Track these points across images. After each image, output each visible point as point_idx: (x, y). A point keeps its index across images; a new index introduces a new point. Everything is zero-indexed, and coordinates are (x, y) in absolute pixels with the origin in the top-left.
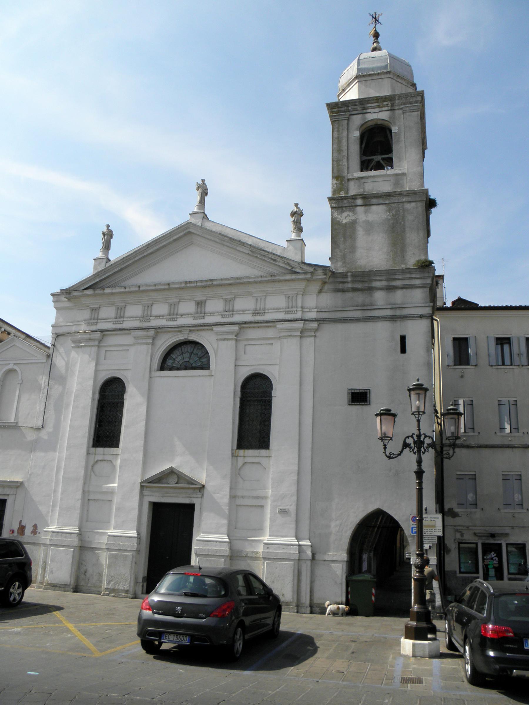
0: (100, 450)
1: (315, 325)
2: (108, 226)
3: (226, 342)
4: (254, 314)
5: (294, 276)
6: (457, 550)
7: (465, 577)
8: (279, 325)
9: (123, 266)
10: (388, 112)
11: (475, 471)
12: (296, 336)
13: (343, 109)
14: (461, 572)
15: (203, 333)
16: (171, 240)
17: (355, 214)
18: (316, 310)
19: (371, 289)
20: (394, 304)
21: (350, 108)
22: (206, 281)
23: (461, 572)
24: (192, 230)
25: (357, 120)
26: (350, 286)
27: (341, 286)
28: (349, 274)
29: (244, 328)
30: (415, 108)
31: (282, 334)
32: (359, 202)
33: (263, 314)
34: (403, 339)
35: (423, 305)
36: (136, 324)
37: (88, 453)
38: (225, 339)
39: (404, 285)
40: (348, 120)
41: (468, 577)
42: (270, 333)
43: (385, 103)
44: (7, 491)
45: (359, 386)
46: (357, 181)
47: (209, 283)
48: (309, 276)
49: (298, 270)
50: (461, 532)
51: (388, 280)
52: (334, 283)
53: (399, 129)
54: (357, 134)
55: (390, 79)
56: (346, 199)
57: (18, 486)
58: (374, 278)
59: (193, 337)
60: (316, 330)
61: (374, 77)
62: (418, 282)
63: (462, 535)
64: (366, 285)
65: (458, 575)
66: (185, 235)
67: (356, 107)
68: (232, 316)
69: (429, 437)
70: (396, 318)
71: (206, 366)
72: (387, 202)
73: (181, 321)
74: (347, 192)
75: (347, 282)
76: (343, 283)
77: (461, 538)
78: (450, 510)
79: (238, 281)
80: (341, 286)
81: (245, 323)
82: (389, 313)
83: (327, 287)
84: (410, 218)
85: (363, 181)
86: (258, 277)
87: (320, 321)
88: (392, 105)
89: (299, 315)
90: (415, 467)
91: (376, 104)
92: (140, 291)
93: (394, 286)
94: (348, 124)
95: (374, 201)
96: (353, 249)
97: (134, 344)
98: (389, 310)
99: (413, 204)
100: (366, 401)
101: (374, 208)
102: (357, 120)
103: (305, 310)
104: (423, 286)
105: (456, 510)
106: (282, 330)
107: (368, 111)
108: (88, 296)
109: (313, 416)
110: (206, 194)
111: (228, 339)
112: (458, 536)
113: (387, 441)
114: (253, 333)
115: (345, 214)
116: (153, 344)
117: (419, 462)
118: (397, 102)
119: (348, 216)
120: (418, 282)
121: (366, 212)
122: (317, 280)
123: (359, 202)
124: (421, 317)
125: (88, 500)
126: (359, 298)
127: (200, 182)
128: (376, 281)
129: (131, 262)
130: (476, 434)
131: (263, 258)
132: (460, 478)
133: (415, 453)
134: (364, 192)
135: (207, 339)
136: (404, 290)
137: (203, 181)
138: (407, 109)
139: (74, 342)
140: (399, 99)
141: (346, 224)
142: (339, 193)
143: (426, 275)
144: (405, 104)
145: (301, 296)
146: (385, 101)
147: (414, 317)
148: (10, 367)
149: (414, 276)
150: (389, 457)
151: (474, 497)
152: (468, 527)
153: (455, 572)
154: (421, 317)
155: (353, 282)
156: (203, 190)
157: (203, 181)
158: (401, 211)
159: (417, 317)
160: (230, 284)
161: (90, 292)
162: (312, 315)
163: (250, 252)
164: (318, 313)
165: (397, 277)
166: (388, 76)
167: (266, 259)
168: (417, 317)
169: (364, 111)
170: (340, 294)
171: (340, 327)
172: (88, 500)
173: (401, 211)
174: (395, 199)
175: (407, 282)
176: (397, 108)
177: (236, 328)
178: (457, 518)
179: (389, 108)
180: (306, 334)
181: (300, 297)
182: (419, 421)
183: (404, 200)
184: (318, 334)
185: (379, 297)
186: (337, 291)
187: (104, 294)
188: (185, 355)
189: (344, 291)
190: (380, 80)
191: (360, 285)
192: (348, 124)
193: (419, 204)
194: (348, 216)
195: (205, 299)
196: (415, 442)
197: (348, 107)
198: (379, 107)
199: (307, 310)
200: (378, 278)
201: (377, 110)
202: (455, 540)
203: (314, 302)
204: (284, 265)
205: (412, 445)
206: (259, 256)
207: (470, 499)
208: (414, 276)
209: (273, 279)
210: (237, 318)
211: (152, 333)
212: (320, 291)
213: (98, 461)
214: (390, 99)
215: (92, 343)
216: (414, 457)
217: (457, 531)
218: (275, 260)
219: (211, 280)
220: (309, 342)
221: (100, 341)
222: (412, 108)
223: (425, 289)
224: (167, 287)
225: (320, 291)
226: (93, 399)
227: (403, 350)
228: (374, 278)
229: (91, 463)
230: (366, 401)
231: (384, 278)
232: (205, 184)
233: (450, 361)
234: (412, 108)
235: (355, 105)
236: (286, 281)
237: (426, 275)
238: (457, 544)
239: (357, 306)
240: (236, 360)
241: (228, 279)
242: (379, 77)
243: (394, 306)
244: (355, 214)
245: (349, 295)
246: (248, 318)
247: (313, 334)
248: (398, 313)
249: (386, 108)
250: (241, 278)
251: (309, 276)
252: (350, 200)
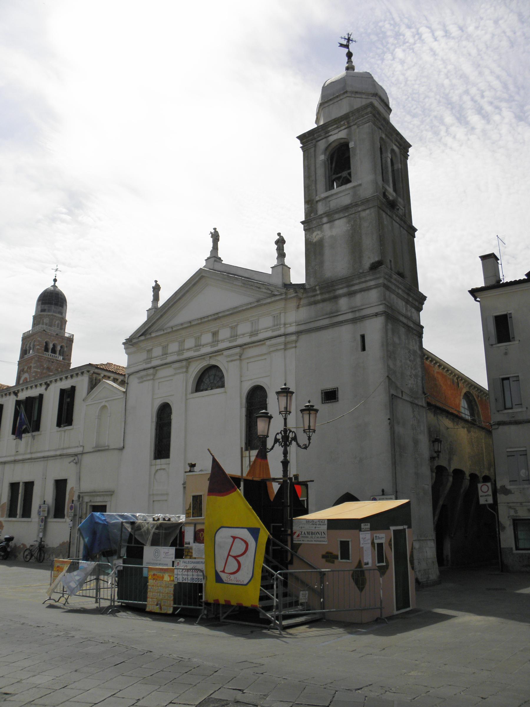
0: (158, 461)
1: (294, 338)
2: (156, 281)
3: (233, 362)
4: (251, 336)
5: (273, 299)
6: (512, 527)
7: (522, 554)
8: (268, 343)
9: (161, 313)
10: (346, 131)
11: (526, 447)
12: (281, 349)
13: (310, 138)
14: (517, 548)
15: (219, 358)
16: (191, 285)
17: (322, 232)
18: (295, 324)
19: (336, 298)
20: (355, 307)
21: (315, 135)
22: (214, 315)
23: (517, 548)
24: (203, 274)
25: (322, 145)
26: (319, 298)
27: (312, 299)
28: (317, 288)
29: (245, 348)
30: (366, 120)
31: (272, 349)
32: (325, 220)
33: (257, 334)
34: (363, 337)
35: (377, 304)
36: (175, 358)
37: (151, 465)
38: (232, 361)
39: (361, 289)
40: (315, 146)
41: (525, 554)
42: (263, 349)
43: (342, 123)
44: (107, 499)
45: (329, 386)
46: (324, 201)
47: (216, 316)
48: (283, 296)
49: (276, 293)
50: (514, 509)
51: (348, 286)
52: (307, 297)
53: (355, 144)
54: (322, 157)
55: (348, 98)
56: (314, 220)
57: (111, 493)
58: (337, 287)
59: (213, 362)
60: (296, 341)
61: (335, 100)
62: (372, 283)
63: (516, 512)
64: (332, 295)
65: (515, 552)
66: (200, 279)
67: (319, 133)
68: (235, 340)
69: (293, 432)
70: (356, 320)
71: (223, 386)
72: (346, 215)
73: (204, 350)
74: (316, 214)
75: (317, 295)
76: (314, 296)
77: (515, 515)
78: (503, 487)
79: (235, 311)
80: (312, 299)
81: (245, 344)
82: (350, 316)
83: (303, 302)
84: (365, 224)
85: (329, 199)
86: (250, 303)
87: (298, 333)
88: (348, 123)
89: (282, 331)
90: (282, 458)
91: (335, 126)
92: (174, 331)
93: (353, 291)
94: (315, 151)
95: (337, 216)
96: (322, 263)
97: (175, 374)
98: (350, 314)
99: (368, 212)
100: (335, 399)
101: (337, 222)
102: (322, 145)
103: (287, 326)
104: (376, 286)
105: (509, 487)
106: (270, 346)
107: (330, 134)
108: (142, 340)
109: (296, 416)
110: (218, 240)
111: (234, 360)
112: (512, 513)
113: (311, 433)
114: (251, 352)
115: (315, 234)
116: (187, 372)
117: (285, 453)
118: (351, 118)
119: (318, 234)
120: (372, 283)
121: (331, 228)
122: (291, 298)
123: (325, 220)
124: (376, 315)
125: (154, 501)
126: (328, 307)
127: (213, 231)
128: (338, 289)
129: (166, 309)
130: (525, 409)
131: (252, 287)
132: (510, 455)
133: (282, 447)
134: (330, 209)
135: (220, 362)
136: (363, 293)
137: (215, 229)
138: (360, 122)
139: (139, 378)
140: (352, 116)
141: (316, 242)
142: (310, 216)
143: (378, 276)
144: (358, 119)
145: (283, 314)
146: (341, 121)
147: (370, 316)
148: (103, 404)
149: (368, 278)
150: (306, 447)
151: (527, 472)
152: (521, 503)
153: (512, 548)
154: (376, 315)
155: (321, 294)
156: (215, 237)
157: (215, 229)
158: (358, 220)
159: (373, 316)
160: (231, 314)
161: (142, 338)
162: (292, 329)
163: (242, 284)
164: (299, 326)
165: (355, 282)
166: (346, 95)
167: (253, 288)
168: (373, 316)
169: (327, 135)
170: (313, 306)
171: (314, 335)
172: (154, 501)
173: (358, 220)
174: (353, 210)
175: (363, 286)
176: (352, 124)
177: (238, 350)
178: (510, 495)
179: (346, 126)
180: (289, 346)
181: (282, 315)
182: (285, 419)
183: (360, 209)
184: (298, 344)
185: (343, 303)
186: (310, 304)
187: (152, 338)
188: (209, 378)
189: (315, 303)
190: (340, 102)
191: (327, 296)
192: (315, 151)
193: (372, 210)
194: (318, 234)
195: (217, 329)
196: (282, 437)
197: (313, 135)
198: (337, 128)
199: (289, 325)
200: (340, 286)
201: (336, 131)
202: (508, 517)
203: (294, 316)
204: (265, 291)
205: (281, 440)
206: (248, 286)
207: (522, 475)
208: (368, 278)
209: (259, 304)
210: (240, 341)
211: (184, 363)
212: (298, 307)
213: (157, 470)
214: (346, 117)
215: (149, 378)
216: (282, 449)
217: (510, 507)
218: (259, 288)
219: (217, 314)
220: (291, 353)
221: (154, 375)
222: (364, 121)
223: (379, 289)
224: (189, 325)
225: (298, 307)
226: (152, 422)
227: (364, 349)
228: (337, 287)
229: (153, 472)
230: (335, 399)
231: (344, 285)
232: (217, 232)
233: (493, 339)
234: (364, 121)
235: (319, 132)
236: (269, 303)
237: (378, 276)
238: (512, 520)
239: (327, 314)
240: (241, 376)
241: (228, 310)
242: (339, 99)
243: (354, 309)
244: (322, 232)
245: (320, 306)
246: (247, 340)
247: (294, 345)
248: (357, 315)
249: (343, 127)
250: (236, 307)
251: (283, 296)
252: (318, 220)
